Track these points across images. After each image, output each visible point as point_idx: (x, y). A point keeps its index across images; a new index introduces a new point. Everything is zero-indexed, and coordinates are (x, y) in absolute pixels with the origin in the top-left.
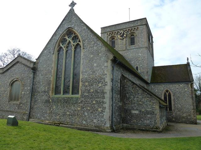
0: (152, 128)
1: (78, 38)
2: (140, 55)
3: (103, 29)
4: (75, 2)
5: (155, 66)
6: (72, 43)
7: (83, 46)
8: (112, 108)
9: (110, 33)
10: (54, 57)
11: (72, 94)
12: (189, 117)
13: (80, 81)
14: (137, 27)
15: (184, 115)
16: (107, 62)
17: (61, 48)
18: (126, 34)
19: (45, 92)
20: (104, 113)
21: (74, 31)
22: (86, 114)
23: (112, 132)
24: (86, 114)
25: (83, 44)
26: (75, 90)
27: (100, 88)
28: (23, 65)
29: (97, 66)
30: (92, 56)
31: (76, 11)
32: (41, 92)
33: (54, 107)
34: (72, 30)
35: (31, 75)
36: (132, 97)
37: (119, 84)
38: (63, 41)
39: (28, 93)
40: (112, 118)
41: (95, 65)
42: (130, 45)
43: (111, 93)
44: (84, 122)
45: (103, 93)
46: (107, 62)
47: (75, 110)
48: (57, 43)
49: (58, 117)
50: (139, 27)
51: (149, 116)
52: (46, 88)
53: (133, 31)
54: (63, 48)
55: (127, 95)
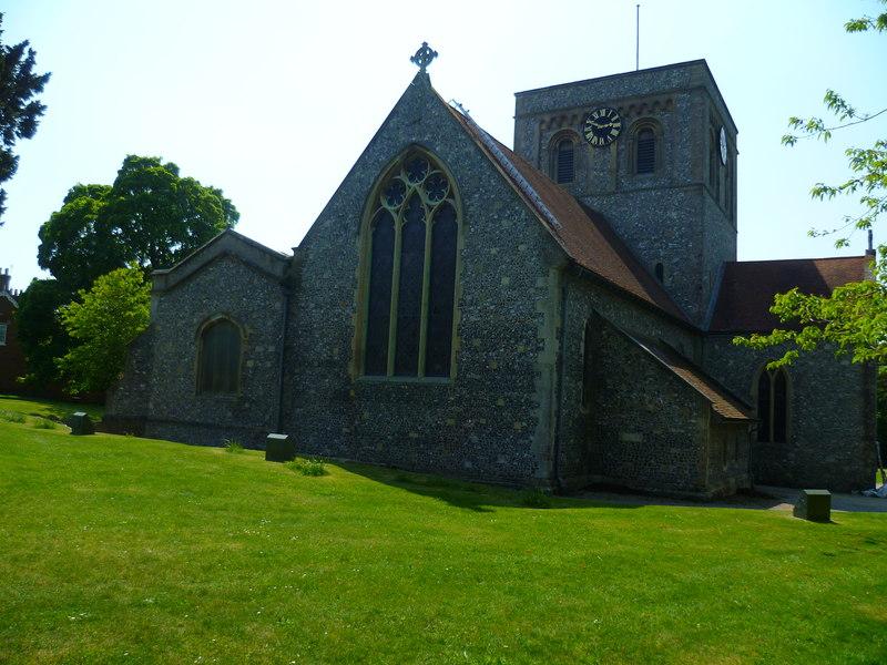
0: (683, 489)
1: (445, 184)
2: (674, 215)
3: (530, 105)
4: (433, 46)
5: (740, 258)
6: (425, 199)
7: (465, 214)
8: (558, 421)
9: (553, 119)
10: (361, 246)
11: (428, 373)
12: (847, 469)
13: (455, 331)
14: (667, 97)
15: (831, 459)
16: (546, 274)
17: (385, 213)
18: (618, 125)
19: (330, 363)
20: (532, 438)
21: (430, 159)
22: (475, 438)
23: (554, 493)
24: (475, 438)
25: (465, 208)
26: (438, 360)
27: (520, 357)
28: (242, 266)
29: (511, 287)
30: (494, 251)
31: (438, 84)
32: (316, 364)
33: (366, 415)
34: (426, 156)
35: (278, 305)
36: (624, 387)
37: (582, 344)
38: (393, 190)
39: (269, 365)
40: (556, 451)
41: (506, 281)
42: (636, 171)
43: (555, 374)
44: (468, 465)
45: (531, 373)
46: (546, 274)
47: (438, 427)
48: (368, 196)
49: (380, 447)
50: (675, 96)
51: (673, 450)
52: (336, 350)
53: (650, 112)
54: (394, 215)
55: (608, 381)
